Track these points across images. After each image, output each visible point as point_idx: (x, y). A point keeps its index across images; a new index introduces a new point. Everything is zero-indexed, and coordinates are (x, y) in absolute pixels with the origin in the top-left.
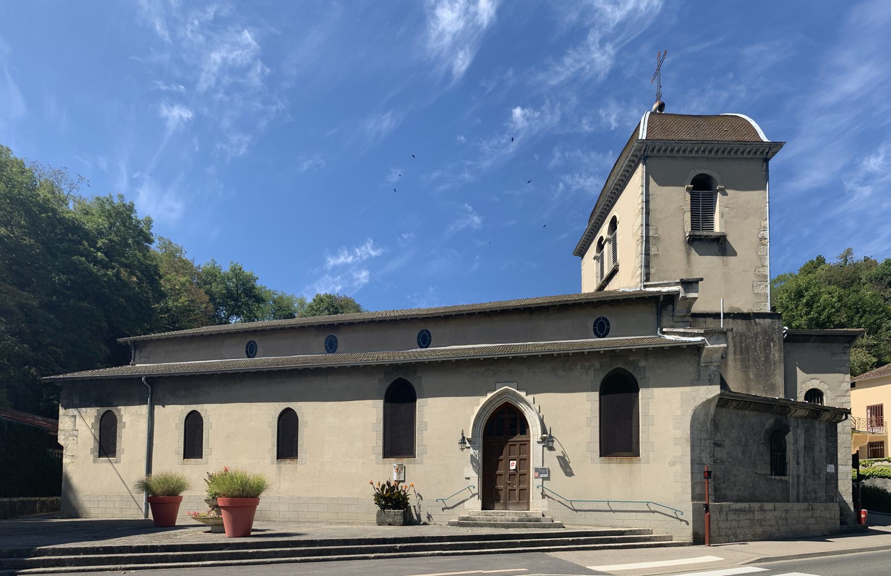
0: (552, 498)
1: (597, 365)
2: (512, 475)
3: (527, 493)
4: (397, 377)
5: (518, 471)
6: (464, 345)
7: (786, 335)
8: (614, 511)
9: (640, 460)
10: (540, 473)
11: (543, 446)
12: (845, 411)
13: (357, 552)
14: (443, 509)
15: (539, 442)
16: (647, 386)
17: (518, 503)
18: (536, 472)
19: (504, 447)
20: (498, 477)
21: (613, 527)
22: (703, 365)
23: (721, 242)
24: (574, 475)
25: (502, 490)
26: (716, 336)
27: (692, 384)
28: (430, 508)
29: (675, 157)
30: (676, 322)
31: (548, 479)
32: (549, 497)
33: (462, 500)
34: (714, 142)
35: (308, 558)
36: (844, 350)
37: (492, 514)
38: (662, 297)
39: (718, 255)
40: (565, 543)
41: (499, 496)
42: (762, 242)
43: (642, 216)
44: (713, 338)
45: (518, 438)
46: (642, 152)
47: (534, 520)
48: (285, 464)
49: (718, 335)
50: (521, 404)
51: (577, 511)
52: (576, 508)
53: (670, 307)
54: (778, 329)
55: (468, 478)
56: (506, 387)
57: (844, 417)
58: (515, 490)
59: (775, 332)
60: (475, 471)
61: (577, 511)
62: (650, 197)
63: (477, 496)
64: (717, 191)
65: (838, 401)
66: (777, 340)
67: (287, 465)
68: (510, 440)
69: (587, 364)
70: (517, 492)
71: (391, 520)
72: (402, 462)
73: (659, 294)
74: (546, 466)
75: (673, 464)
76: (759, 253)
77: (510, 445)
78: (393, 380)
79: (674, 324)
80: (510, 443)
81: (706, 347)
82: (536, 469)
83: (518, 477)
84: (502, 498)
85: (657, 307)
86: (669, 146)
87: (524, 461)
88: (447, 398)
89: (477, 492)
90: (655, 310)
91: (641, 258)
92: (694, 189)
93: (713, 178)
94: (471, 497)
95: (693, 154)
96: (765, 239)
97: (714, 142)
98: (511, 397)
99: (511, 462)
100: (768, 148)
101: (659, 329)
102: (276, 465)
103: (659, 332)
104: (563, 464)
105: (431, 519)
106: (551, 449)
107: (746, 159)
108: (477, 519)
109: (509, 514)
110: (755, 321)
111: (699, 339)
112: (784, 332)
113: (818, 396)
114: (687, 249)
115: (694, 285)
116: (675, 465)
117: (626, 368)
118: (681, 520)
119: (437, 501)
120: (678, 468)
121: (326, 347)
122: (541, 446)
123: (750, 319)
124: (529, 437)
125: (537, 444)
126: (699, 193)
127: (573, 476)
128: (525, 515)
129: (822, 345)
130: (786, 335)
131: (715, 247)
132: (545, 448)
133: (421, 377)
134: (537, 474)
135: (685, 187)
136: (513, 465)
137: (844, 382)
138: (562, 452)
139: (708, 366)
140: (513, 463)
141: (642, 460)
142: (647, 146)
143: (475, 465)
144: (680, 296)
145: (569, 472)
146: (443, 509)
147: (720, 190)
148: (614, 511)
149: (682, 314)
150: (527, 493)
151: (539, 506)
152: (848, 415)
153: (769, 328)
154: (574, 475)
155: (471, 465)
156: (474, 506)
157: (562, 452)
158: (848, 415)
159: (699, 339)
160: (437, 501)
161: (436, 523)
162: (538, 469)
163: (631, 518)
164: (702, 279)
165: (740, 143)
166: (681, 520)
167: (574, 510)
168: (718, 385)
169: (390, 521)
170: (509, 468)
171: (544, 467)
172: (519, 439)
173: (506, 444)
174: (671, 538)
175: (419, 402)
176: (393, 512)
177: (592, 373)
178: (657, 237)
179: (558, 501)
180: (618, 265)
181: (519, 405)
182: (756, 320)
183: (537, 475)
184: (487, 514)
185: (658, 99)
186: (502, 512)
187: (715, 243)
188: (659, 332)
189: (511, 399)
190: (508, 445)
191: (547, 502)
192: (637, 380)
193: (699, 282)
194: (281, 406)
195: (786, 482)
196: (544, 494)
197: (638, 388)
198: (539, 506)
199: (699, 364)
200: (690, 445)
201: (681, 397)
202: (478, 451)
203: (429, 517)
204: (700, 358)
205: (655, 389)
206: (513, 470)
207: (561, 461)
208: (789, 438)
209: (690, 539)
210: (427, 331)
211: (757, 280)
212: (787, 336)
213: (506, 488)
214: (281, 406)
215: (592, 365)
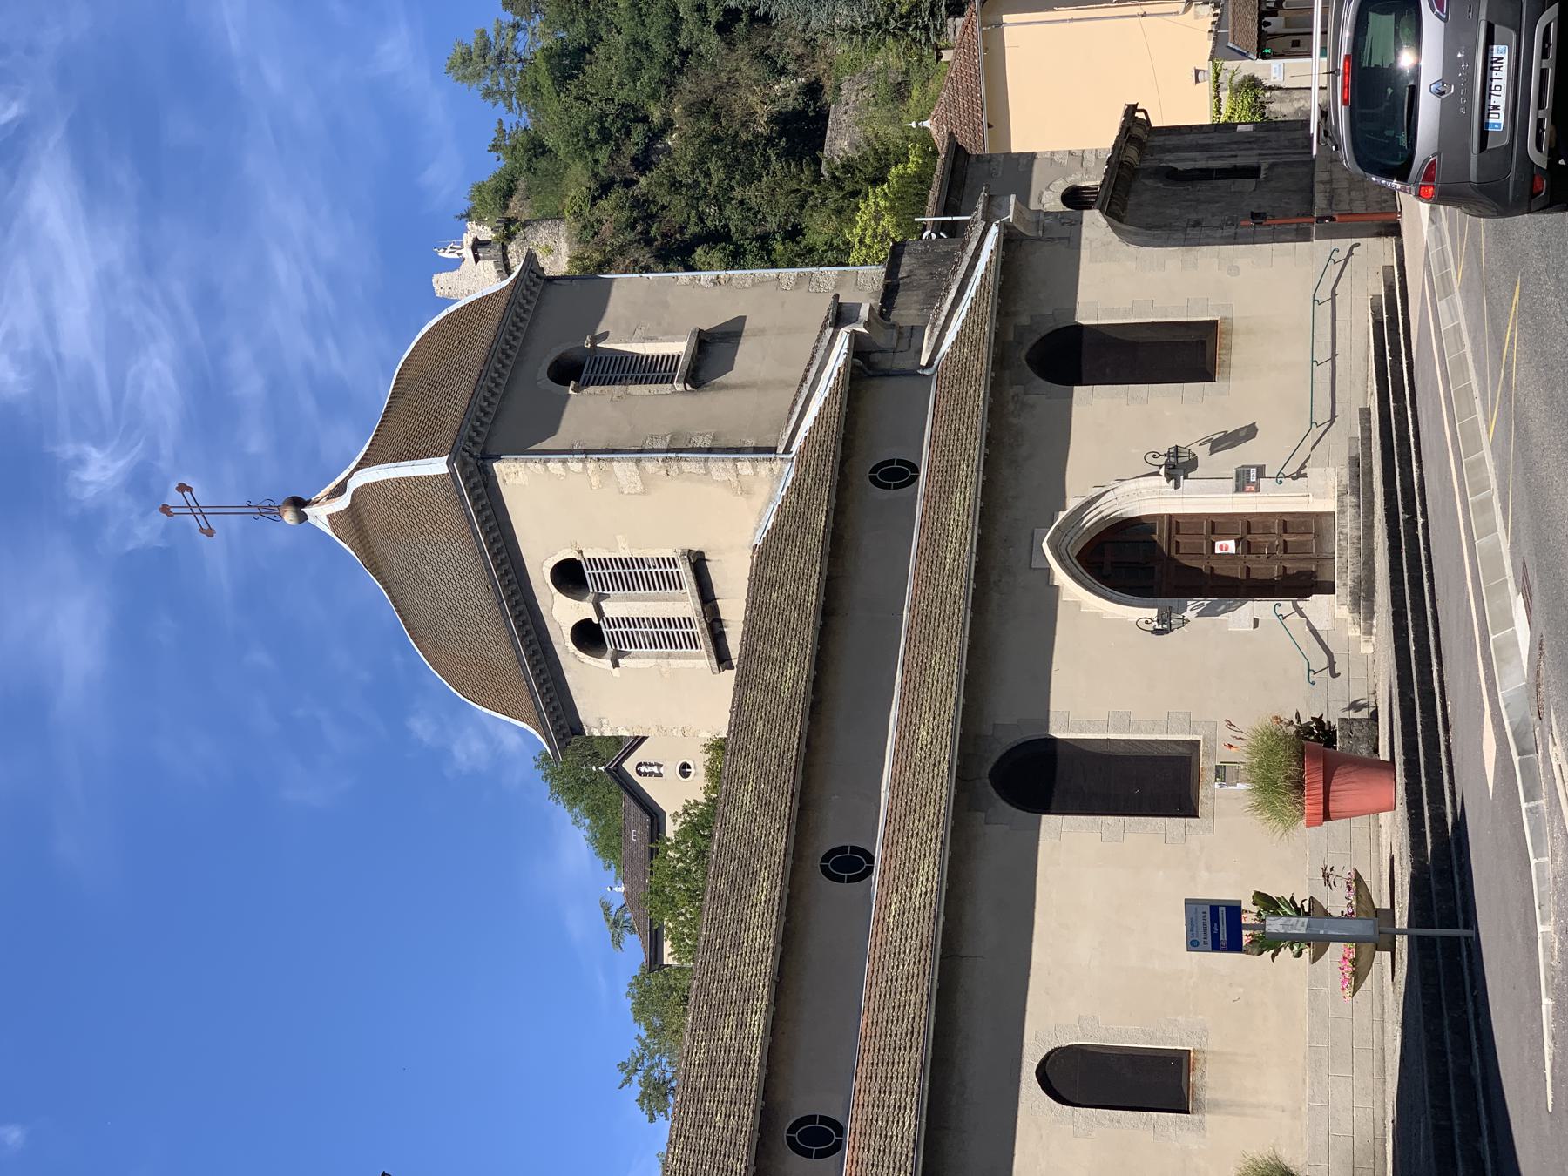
0: (1306, 462)
1: (1017, 389)
2: (1246, 546)
4: (987, 781)
6: (884, 761)
7: (942, 234)
8: (1334, 355)
9: (1226, 318)
12: (1131, 111)
13: (1416, 574)
14: (1334, 675)
15: (1177, 486)
17: (1317, 535)
22: (1040, 232)
23: (708, 340)
24: (1254, 423)
26: (994, 208)
28: (1330, 705)
30: (910, 346)
32: (1303, 466)
36: (983, 162)
37: (1344, 559)
38: (857, 360)
39: (738, 343)
40: (1401, 412)
41: (1300, 573)
42: (722, 282)
43: (618, 460)
44: (997, 212)
45: (1160, 537)
46: (471, 460)
47: (1355, 469)
48: (1203, 1087)
49: (993, 206)
50: (1084, 522)
52: (1328, 417)
53: (876, 357)
54: (926, 246)
55: (1256, 623)
57: (1140, 115)
58: (1285, 542)
59: (933, 250)
60: (1239, 607)
63: (1300, 604)
67: (1207, 1081)
68: (1165, 549)
69: (1011, 407)
71: (1365, 746)
72: (1210, 769)
73: (850, 366)
74: (1233, 473)
75: (1235, 270)
77: (1178, 552)
78: (992, 790)
83: (1254, 536)
84: (1304, 566)
85: (870, 377)
87: (1216, 525)
88: (1054, 668)
89: (1291, 602)
90: (876, 382)
92: (577, 381)
93: (563, 354)
94: (1302, 615)
95: (503, 382)
96: (718, 277)
98: (1068, 538)
99: (1218, 551)
101: (920, 372)
102: (1208, 1117)
103: (927, 372)
105: (1362, 702)
106: (1192, 464)
107: (537, 308)
108: (1356, 575)
109: (1343, 527)
111: (994, 230)
112: (934, 236)
113: (1078, 193)
114: (711, 390)
115: (843, 309)
116: (1238, 267)
117: (1029, 345)
118: (1350, 254)
120: (1241, 262)
121: (821, 1155)
123: (898, 285)
127: (1257, 425)
130: (942, 234)
131: (718, 349)
132: (1190, 475)
134: (1248, 488)
135: (569, 395)
138: (1201, 445)
139: (1043, 227)
140: (1221, 547)
141: (1223, 315)
143: (1223, 607)
144: (864, 330)
145: (1250, 432)
146: (1334, 675)
148: (1334, 355)
149: (895, 335)
151: (1324, 482)
153: (921, 258)
154: (1254, 423)
155: (1222, 617)
156: (1325, 610)
157: (1201, 445)
159: (994, 230)
160: (1313, 683)
161: (1370, 691)
163: (1348, 329)
164: (837, 296)
165: (508, 311)
166: (1350, 254)
167: (1332, 421)
168: (1082, 214)
169: (1367, 748)
170: (1232, 554)
171: (1234, 476)
172: (1165, 535)
173: (1175, 560)
174: (1388, 270)
175: (1058, 732)
176: (1342, 741)
177: (1031, 399)
178: (672, 437)
181: (1088, 525)
182: (900, 276)
183: (1253, 488)
184: (1345, 570)
186: (1339, 540)
187: (710, 348)
188: (927, 372)
190: (1177, 557)
191: (1314, 469)
192: (1055, 328)
195: (1272, 166)
196: (1295, 475)
198: (1324, 482)
199: (1040, 239)
200: (1198, 247)
201: (1100, 262)
202: (1189, 603)
203: (1355, 706)
205: (1080, 299)
206: (1237, 546)
207: (1220, 447)
208: (1180, 166)
209: (1389, 243)
210: (826, 858)
211: (806, 286)
213: (1281, 560)
215: (1016, 398)
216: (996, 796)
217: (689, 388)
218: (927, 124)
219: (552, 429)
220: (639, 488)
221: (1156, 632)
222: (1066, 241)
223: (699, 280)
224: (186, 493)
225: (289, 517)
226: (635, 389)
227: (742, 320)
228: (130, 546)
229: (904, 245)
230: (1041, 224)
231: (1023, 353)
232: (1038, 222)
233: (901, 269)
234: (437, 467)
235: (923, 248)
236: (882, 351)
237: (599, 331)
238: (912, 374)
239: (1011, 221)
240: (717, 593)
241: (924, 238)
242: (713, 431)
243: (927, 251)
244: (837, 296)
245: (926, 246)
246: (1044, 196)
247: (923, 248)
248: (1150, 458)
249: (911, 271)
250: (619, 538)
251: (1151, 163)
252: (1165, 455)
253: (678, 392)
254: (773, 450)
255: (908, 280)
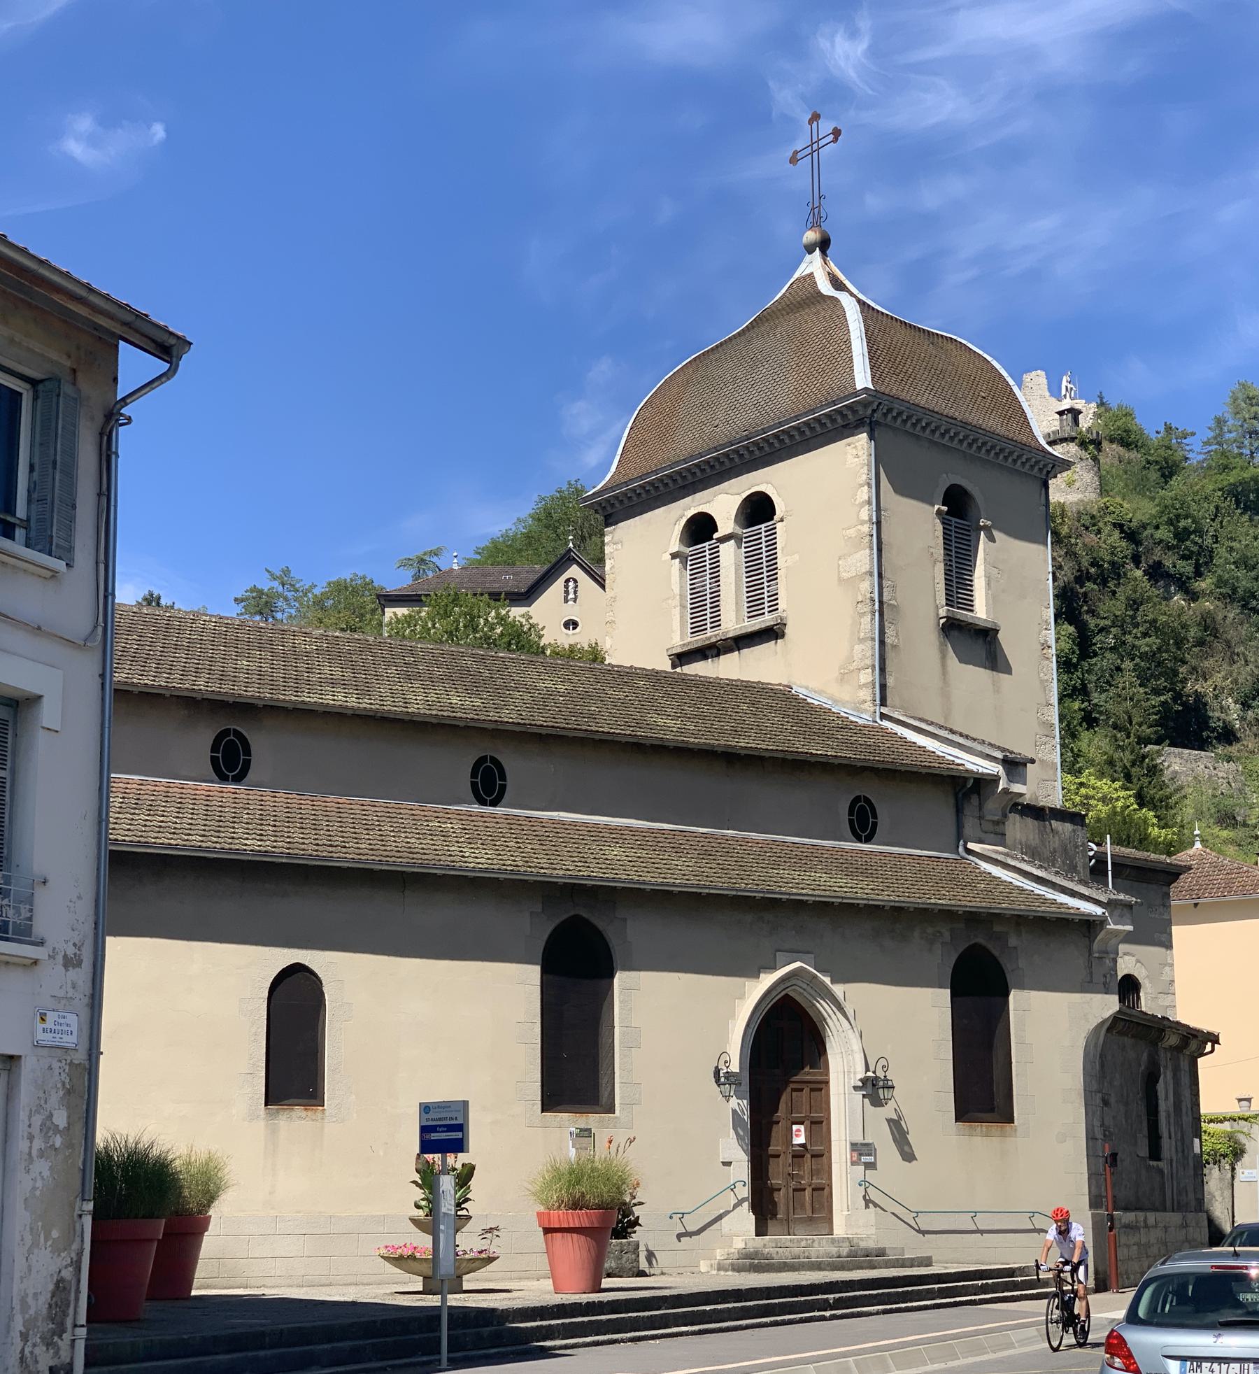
1: (947, 935)
2: (799, 1154)
3: (825, 1197)
4: (572, 913)
5: (809, 1148)
7: (1093, 861)
8: (982, 1232)
9: (1016, 1130)
10: (861, 1155)
11: (864, 1096)
12: (1212, 1038)
14: (679, 1236)
15: (855, 1088)
16: (1022, 987)
17: (811, 1219)
18: (853, 1150)
19: (782, 1094)
20: (771, 1159)
21: (1002, 1264)
22: (1097, 955)
23: (989, 639)
25: (780, 1189)
26: (1120, 910)
27: (1083, 989)
29: (917, 437)
30: (986, 833)
31: (870, 1166)
32: (876, 1205)
33: (717, 1213)
34: (980, 431)
35: (958, 1299)
37: (788, 1244)
38: (972, 781)
39: (985, 668)
41: (775, 1204)
42: (1045, 651)
43: (871, 554)
44: (1117, 912)
45: (807, 1074)
46: (869, 412)
50: (821, 1001)
51: (924, 1233)
53: (974, 800)
56: (798, 964)
57: (1208, 1047)
59: (1078, 853)
61: (924, 1233)
62: (882, 512)
63: (746, 1205)
64: (980, 528)
65: (1160, 1002)
66: (1081, 870)
67: (295, 1120)
69: (930, 930)
70: (808, 1193)
71: (613, 1265)
76: (1042, 675)
78: (565, 917)
79: (983, 836)
80: (792, 1086)
81: (1108, 927)
82: (852, 1144)
83: (809, 1161)
85: (956, 795)
86: (1033, 457)
87: (819, 1125)
90: (952, 801)
91: (873, 648)
92: (948, 513)
94: (735, 1206)
95: (946, 440)
96: (1049, 647)
97: (980, 431)
98: (805, 986)
99: (795, 1127)
100: (1051, 466)
103: (961, 849)
104: (897, 1136)
105: (654, 1262)
106: (877, 1102)
108: (774, 1256)
109: (819, 1243)
110: (1051, 825)
111: (1099, 911)
112: (1091, 853)
115: (1021, 768)
117: (990, 946)
119: (671, 1217)
121: (214, 761)
122: (859, 1095)
123: (1044, 821)
124: (827, 1074)
125: (854, 1092)
126: (951, 521)
128: (848, 1244)
129: (1136, 884)
130: (1093, 861)
131: (979, 648)
132: (866, 1100)
133: (625, 920)
134: (855, 1154)
136: (800, 1137)
137: (1166, 965)
138: (895, 1110)
139: (1102, 958)
140: (798, 1130)
142: (880, 403)
143: (741, 1133)
144: (1001, 787)
145: (908, 1156)
146: (679, 1236)
147: (985, 528)
148: (982, 1232)
149: (996, 818)
150: (825, 1197)
152: (1216, 1045)
157: (895, 1110)
158: (1216, 1045)
159: (1099, 911)
160: (671, 1217)
161: (665, 1270)
162: (856, 1144)
164: (1033, 761)
167: (919, 1231)
169: (611, 1267)
171: (866, 1141)
172: (808, 1078)
179: (893, 1213)
180: (785, 625)
182: (1052, 822)
183: (855, 1159)
184: (779, 1245)
185: (816, 220)
186: (806, 1240)
187: (981, 641)
188: (961, 849)
189: (804, 990)
190: (789, 1089)
191: (873, 1215)
193: (1028, 765)
194: (284, 957)
195: (1161, 1172)
196: (867, 1198)
197: (1008, 987)
199: (1090, 954)
204: (1092, 942)
208: (1160, 1086)
211: (1041, 733)
212: (1095, 863)
213: (787, 1186)
214: (284, 957)
216: (558, 922)
217: (942, 621)
218: (1198, 845)
219: (902, 489)
220: (845, 575)
221: (717, 1071)
222: (1088, 979)
223: (1046, 629)
224: (832, 136)
225: (811, 236)
226: (940, 569)
227: (1008, 670)
228: (771, 84)
229: (1082, 826)
230: (1105, 955)
231: (981, 940)
232: (1107, 953)
233: (1059, 823)
234: (862, 378)
235: (1080, 844)
236: (981, 807)
237: (996, 533)
238: (959, 835)
239: (1108, 927)
240: (745, 651)
241: (1090, 844)
242: (901, 646)
243: (1077, 847)
244: (1033, 761)
245: (1081, 846)
246: (1131, 957)
247: (1080, 844)
248: (883, 1062)
249: (1057, 833)
250: (796, 557)
251: (1163, 1058)
252: (885, 1077)
253: (938, 611)
254: (883, 702)
255: (1048, 830)
